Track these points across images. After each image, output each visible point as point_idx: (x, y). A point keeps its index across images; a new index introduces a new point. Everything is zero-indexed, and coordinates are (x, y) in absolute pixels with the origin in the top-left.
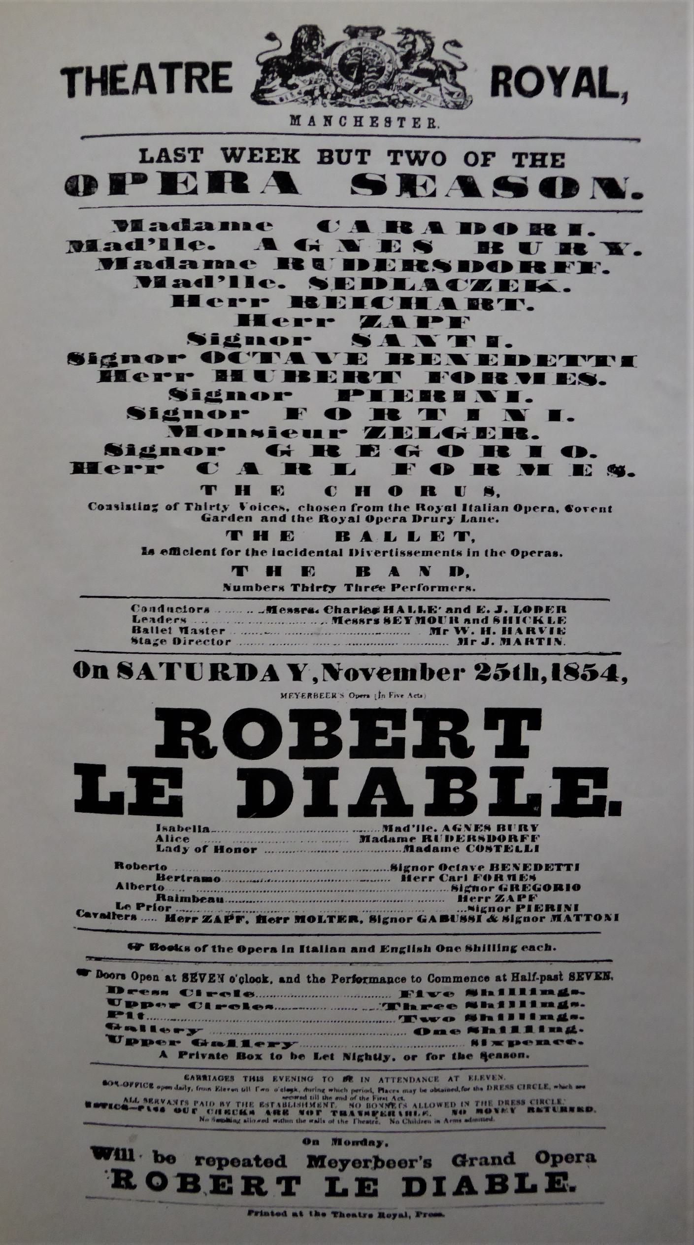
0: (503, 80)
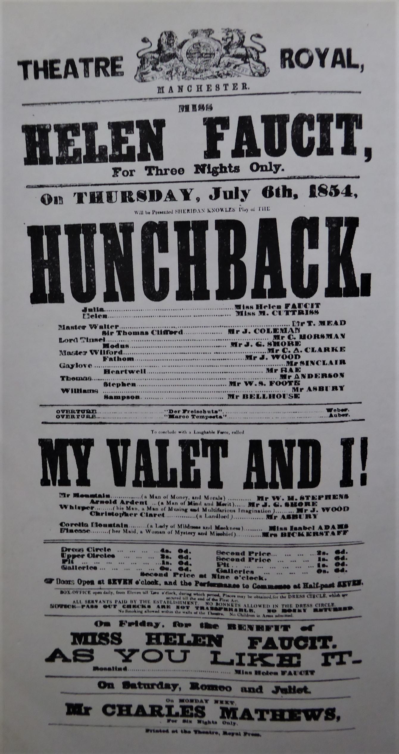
0: (289, 58)
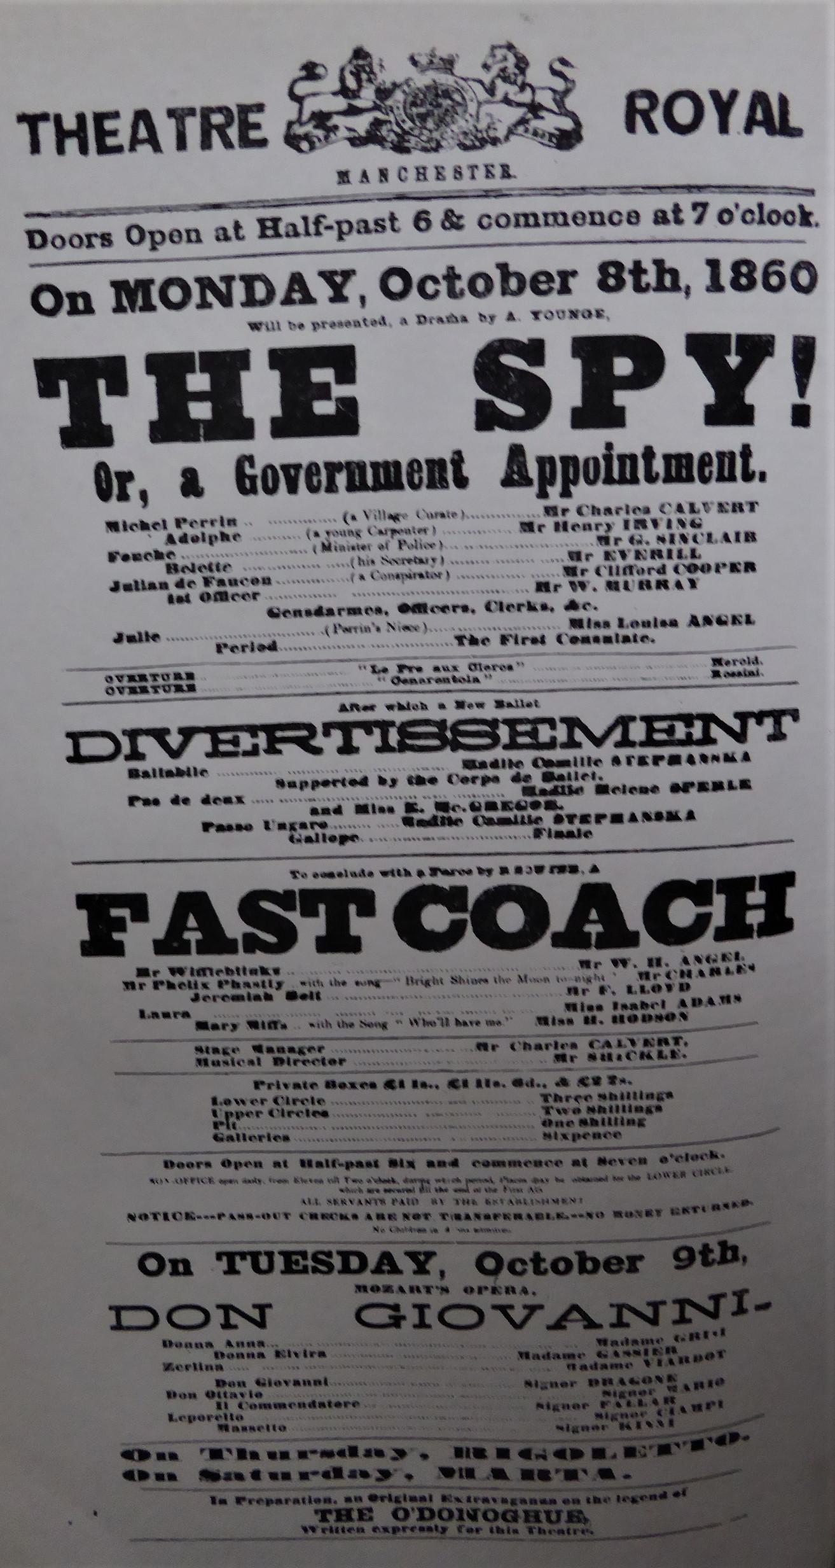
0: (639, 110)
